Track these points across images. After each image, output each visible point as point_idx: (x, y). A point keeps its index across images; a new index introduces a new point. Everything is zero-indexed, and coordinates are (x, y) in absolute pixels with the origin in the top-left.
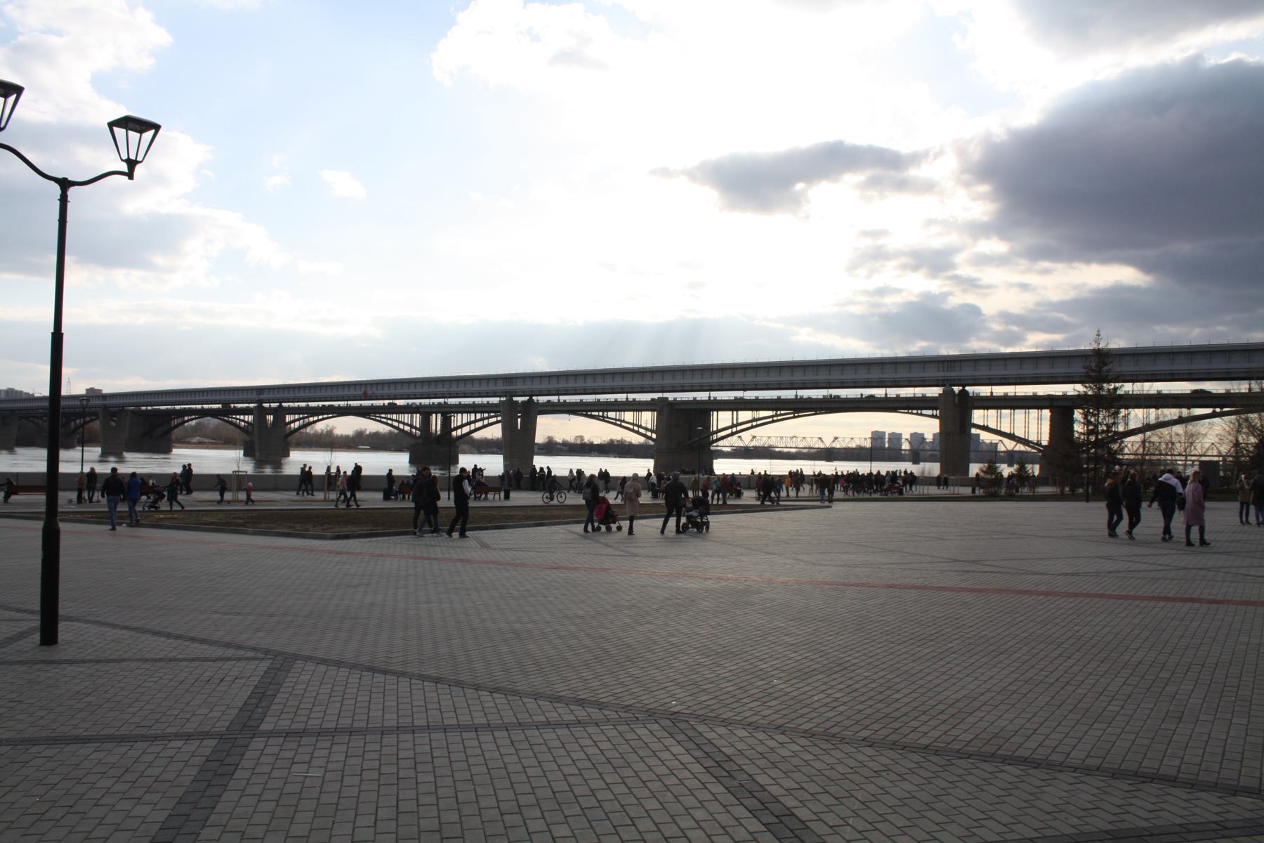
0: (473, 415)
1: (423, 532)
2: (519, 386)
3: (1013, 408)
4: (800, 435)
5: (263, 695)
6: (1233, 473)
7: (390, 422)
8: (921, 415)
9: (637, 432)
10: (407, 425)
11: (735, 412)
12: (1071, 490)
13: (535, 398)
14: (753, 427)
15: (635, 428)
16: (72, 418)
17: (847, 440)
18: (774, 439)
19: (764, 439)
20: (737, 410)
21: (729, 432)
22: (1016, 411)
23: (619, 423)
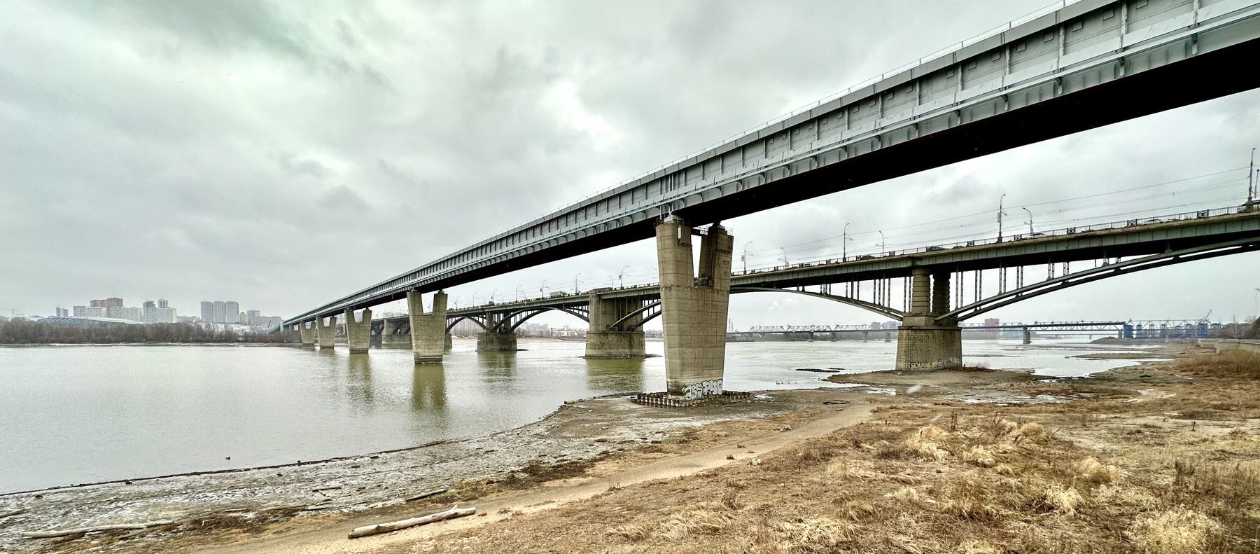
0: (650, 301)
18: (844, 327)
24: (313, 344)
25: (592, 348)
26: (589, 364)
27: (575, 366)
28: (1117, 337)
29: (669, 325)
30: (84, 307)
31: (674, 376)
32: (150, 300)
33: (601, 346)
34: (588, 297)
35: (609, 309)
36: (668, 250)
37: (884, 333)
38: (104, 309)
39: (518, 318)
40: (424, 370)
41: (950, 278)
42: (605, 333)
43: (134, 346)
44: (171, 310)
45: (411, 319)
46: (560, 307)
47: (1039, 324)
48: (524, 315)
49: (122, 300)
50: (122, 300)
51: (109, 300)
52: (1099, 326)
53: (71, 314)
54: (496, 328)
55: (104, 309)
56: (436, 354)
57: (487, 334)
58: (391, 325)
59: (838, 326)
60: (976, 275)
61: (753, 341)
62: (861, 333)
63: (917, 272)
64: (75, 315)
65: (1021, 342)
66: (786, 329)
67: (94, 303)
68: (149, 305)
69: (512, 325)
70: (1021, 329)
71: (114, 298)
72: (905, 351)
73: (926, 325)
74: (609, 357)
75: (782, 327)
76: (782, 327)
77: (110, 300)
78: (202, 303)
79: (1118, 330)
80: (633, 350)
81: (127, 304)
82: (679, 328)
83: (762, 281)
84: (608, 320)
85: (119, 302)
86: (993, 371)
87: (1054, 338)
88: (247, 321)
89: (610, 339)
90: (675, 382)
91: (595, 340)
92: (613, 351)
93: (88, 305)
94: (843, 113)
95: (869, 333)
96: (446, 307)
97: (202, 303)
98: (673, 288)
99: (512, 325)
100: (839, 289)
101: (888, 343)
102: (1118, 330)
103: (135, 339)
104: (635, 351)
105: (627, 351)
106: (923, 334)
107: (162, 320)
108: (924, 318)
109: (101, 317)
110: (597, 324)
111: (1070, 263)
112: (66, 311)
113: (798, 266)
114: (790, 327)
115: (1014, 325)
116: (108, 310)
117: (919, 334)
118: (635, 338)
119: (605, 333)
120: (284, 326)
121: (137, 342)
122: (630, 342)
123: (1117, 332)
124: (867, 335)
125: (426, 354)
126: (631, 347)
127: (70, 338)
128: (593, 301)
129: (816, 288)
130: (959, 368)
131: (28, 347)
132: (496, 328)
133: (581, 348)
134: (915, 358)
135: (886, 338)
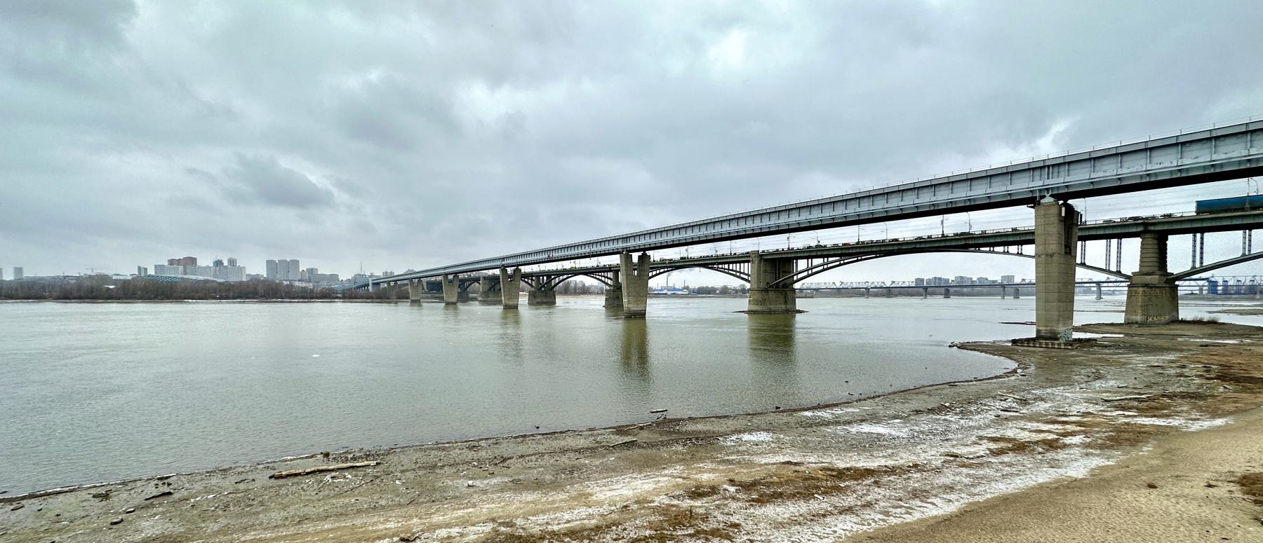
0: (826, 259)
1: (792, 352)
2: (631, 243)
3: (1120, 236)
4: (871, 281)
5: (1164, 453)
6: (1080, 225)
7: (603, 279)
8: (993, 252)
9: (739, 277)
10: (738, 272)
11: (1198, 235)
12: (1062, 204)
13: (648, 253)
14: (809, 276)
15: (738, 274)
16: (553, 277)
17: (900, 283)
18: (900, 283)
19: (849, 284)
20: (1110, 238)
21: (806, 274)
22: (1123, 240)
23: (727, 272)
24: (420, 301)
25: (754, 304)
26: (750, 319)
27: (737, 321)
28: (1198, 292)
29: (1047, 284)
30: (164, 266)
31: (1049, 324)
32: (220, 259)
33: (763, 302)
34: (749, 256)
35: (769, 268)
36: (1053, 226)
37: (943, 289)
38: (181, 268)
39: (557, 280)
40: (633, 322)
41: (1167, 240)
42: (766, 290)
43: (298, 302)
44: (241, 268)
45: (501, 278)
46: (705, 266)
47: (1027, 281)
48: (565, 276)
49: (298, 261)
50: (298, 261)
51: (184, 258)
52: (1115, 284)
53: (151, 272)
54: (541, 288)
55: (181, 268)
56: (641, 309)
57: (614, 291)
58: (487, 282)
59: (894, 282)
60: (1195, 241)
61: (812, 297)
62: (921, 289)
63: (1148, 236)
64: (156, 273)
65: (1094, 297)
66: (838, 285)
67: (172, 262)
68: (218, 263)
69: (553, 284)
70: (1094, 285)
71: (190, 257)
72: (1141, 306)
73: (1159, 283)
74: (770, 312)
75: (834, 283)
76: (834, 283)
77: (185, 259)
78: (267, 261)
79: (1199, 286)
80: (788, 306)
81: (202, 262)
82: (1058, 287)
83: (963, 243)
84: (769, 278)
85: (192, 261)
86: (1224, 324)
87: (1111, 294)
88: (307, 278)
89: (770, 296)
90: (1051, 330)
91: (758, 296)
92: (773, 307)
93: (166, 263)
94: (1211, 141)
95: (929, 289)
96: (298, 268)
97: (267, 261)
98: (1055, 255)
99: (553, 284)
100: (1013, 249)
101: (947, 299)
102: (1199, 286)
103: (250, 295)
104: (789, 306)
105: (783, 307)
106: (1158, 290)
107: (233, 279)
108: (1157, 276)
109: (178, 274)
110: (759, 282)
111: (1253, 231)
112: (146, 269)
113: (1011, 230)
114: (843, 283)
115: (1084, 281)
116: (185, 268)
117: (1154, 291)
118: (789, 294)
119: (766, 290)
120: (373, 284)
121: (251, 298)
122: (785, 298)
123: (1198, 288)
124: (926, 291)
125: (635, 309)
126: (786, 303)
127: (198, 294)
128: (756, 260)
129: (1000, 249)
130: (1177, 321)
131: (137, 302)
132: (541, 288)
133: (744, 304)
134: (1151, 312)
135: (945, 295)
